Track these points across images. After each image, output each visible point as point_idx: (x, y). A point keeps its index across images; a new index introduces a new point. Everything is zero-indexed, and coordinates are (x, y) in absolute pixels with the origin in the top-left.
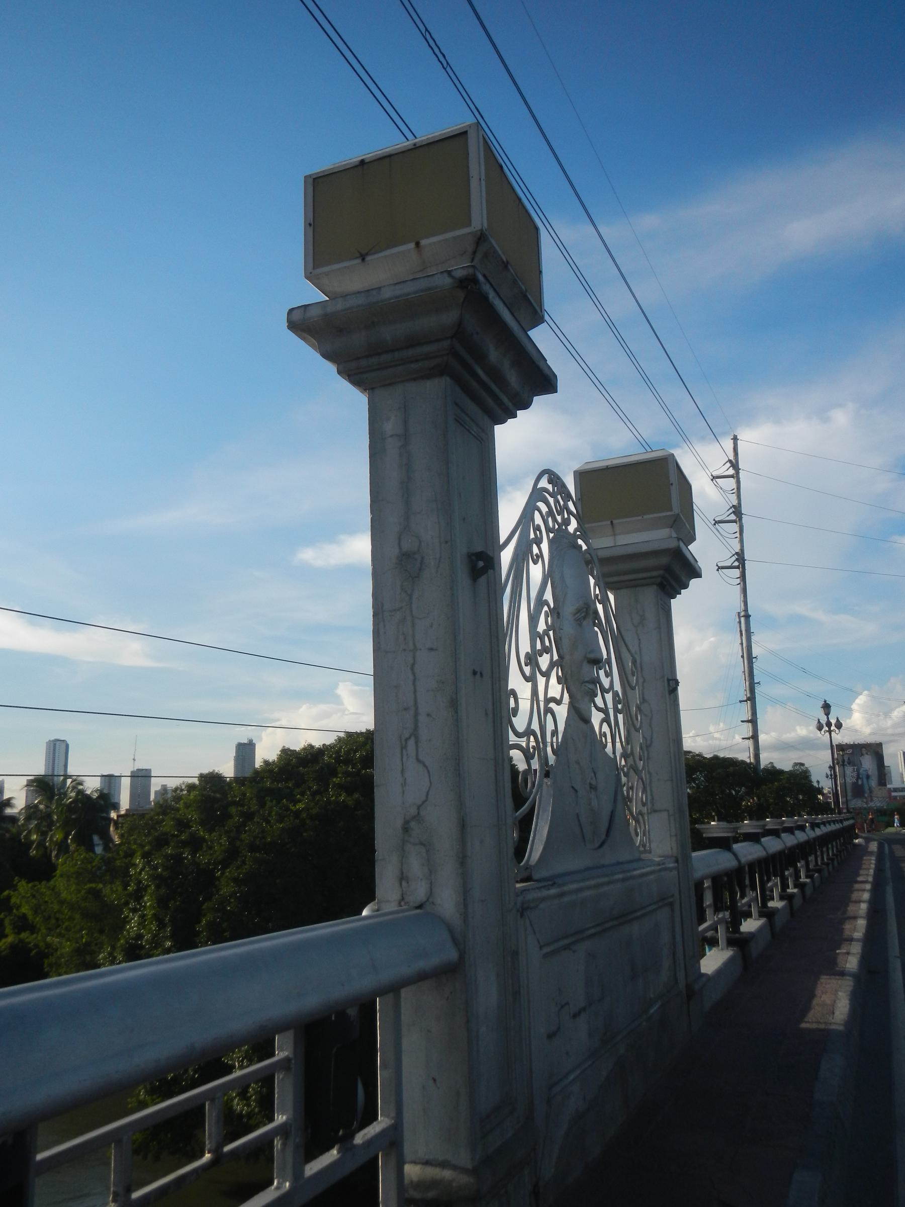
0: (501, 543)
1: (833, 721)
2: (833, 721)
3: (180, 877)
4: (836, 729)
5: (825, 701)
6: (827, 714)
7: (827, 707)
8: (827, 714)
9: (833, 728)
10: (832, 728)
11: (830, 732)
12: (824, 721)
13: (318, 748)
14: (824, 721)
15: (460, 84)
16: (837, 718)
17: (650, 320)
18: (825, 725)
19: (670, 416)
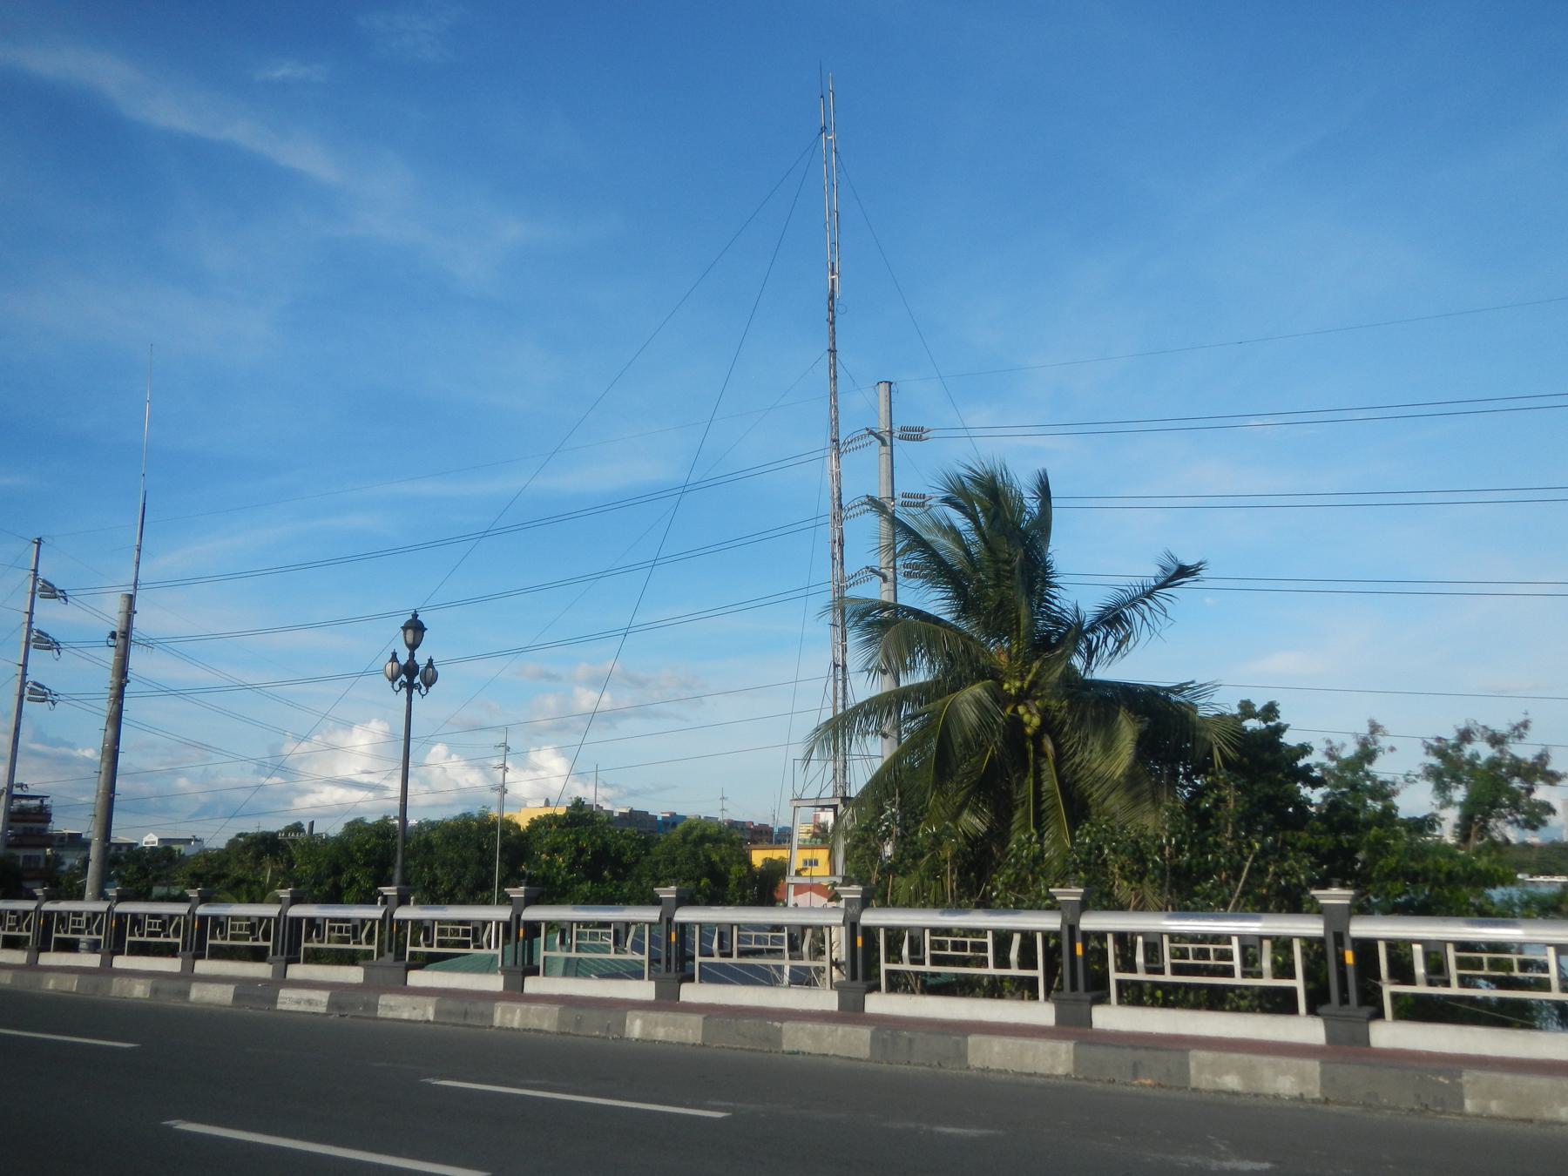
8: (413, 647)
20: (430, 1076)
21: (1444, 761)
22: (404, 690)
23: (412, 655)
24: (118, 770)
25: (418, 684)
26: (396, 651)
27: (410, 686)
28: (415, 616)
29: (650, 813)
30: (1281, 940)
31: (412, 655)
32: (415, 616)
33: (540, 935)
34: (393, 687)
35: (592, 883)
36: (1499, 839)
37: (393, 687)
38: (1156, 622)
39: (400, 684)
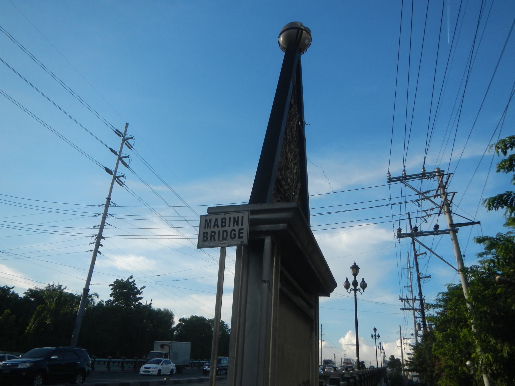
0: (172, 327)
1: (377, 335)
2: (377, 335)
3: (163, 325)
4: (361, 289)
5: (375, 327)
6: (355, 274)
7: (375, 330)
8: (355, 274)
9: (358, 287)
10: (357, 288)
11: (376, 338)
12: (374, 335)
13: (16, 294)
14: (374, 335)
15: (471, 64)
16: (363, 279)
17: (130, 143)
18: (374, 336)
19: (23, 48)
23: (355, 278)
28: (355, 263)
31: (355, 278)
32: (355, 263)
39: (350, 290)
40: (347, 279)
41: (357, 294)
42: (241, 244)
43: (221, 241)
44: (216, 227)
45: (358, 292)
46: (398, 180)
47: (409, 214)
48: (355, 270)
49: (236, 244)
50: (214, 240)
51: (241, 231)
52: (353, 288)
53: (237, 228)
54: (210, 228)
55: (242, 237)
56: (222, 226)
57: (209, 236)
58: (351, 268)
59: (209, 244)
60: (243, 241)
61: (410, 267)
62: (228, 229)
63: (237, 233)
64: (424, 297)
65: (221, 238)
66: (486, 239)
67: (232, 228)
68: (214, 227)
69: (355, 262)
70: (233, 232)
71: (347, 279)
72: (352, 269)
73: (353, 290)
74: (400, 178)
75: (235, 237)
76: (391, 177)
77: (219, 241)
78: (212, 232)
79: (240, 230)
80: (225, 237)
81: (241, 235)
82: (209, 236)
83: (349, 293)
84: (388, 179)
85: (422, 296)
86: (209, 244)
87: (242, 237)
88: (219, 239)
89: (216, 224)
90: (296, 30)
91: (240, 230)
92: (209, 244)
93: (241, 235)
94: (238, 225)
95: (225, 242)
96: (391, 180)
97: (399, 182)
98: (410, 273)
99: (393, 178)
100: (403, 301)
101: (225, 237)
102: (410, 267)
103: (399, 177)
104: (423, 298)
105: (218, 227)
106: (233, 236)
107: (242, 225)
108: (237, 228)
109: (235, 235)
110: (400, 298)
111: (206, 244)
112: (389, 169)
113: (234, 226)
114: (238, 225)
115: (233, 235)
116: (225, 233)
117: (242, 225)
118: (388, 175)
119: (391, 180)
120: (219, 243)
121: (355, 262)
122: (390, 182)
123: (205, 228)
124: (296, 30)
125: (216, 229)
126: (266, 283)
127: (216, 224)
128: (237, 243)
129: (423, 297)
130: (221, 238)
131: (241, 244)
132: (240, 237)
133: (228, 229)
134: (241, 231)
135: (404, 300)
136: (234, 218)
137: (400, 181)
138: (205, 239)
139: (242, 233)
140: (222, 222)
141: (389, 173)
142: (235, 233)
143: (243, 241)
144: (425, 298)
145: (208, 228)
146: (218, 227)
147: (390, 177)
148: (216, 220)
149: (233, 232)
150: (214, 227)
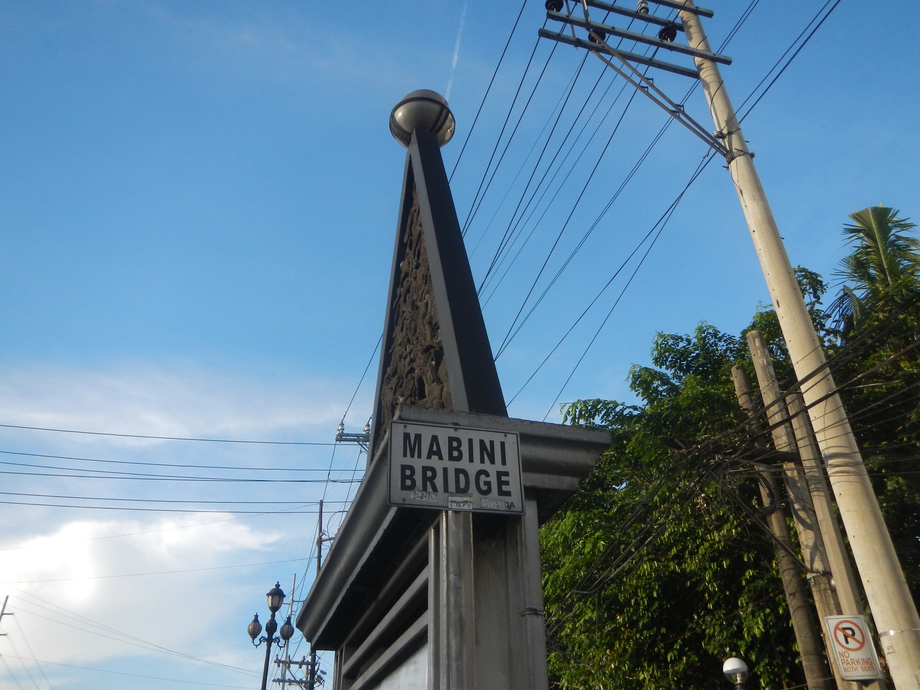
6: (274, 609)
8: (274, 609)
20: (789, 487)
21: (651, 402)
22: (264, 645)
23: (273, 616)
24: (809, 373)
25: (278, 638)
26: (258, 614)
27: (270, 641)
28: (278, 586)
29: (726, 119)
30: (851, 552)
31: (273, 616)
32: (278, 586)
33: (838, 615)
34: (253, 642)
35: (754, 636)
36: (770, 542)
37: (253, 642)
38: (857, 238)
39: (260, 640)
40: (256, 616)
41: (272, 648)
42: (507, 509)
43: (452, 494)
44: (435, 458)
45: (274, 645)
46: (355, 440)
47: (321, 503)
48: (277, 598)
49: (496, 508)
50: (435, 489)
51: (504, 478)
52: (266, 636)
53: (492, 469)
54: (420, 456)
55: (508, 494)
56: (451, 458)
57: (418, 477)
58: (268, 595)
59: (422, 498)
60: (512, 503)
61: (293, 601)
62: (472, 469)
63: (493, 479)
64: (319, 658)
65: (452, 487)
66: (625, 559)
67: (477, 466)
68: (429, 457)
69: (278, 582)
70: (483, 478)
71: (256, 616)
72: (270, 597)
73: (266, 640)
74: (358, 437)
75: (489, 491)
76: (344, 432)
77: (446, 494)
78: (425, 469)
79: (500, 474)
80: (462, 485)
81: (505, 488)
82: (418, 477)
83: (257, 646)
84: (338, 435)
85: (316, 657)
86: (422, 498)
87: (508, 494)
88: (446, 490)
89: (435, 449)
90: (437, 108)
91: (500, 474)
92: (420, 499)
93: (505, 488)
94: (492, 461)
95: (465, 499)
96: (342, 437)
97: (356, 443)
98: (292, 611)
99: (348, 435)
100: (281, 664)
101: (462, 485)
102: (293, 600)
103: (358, 436)
104: (316, 660)
105: (441, 458)
106: (484, 488)
107: (504, 462)
108: (492, 469)
109: (488, 484)
110: (277, 658)
111: (412, 497)
112: (344, 416)
113: (482, 461)
114: (492, 461)
115: (485, 485)
116: (462, 477)
117: (504, 462)
118: (340, 428)
119: (342, 437)
120: (450, 498)
121: (278, 582)
122: (340, 441)
123: (405, 455)
124: (437, 108)
125: (434, 462)
126: (539, 616)
127: (435, 449)
128: (497, 506)
129: (317, 658)
130: (452, 487)
131: (507, 509)
132: (501, 493)
133: (472, 469)
134: (504, 478)
135: (283, 662)
136: (482, 442)
137: (358, 442)
138: (408, 483)
139: (507, 483)
140: (451, 449)
141: (342, 424)
142: (488, 479)
143: (512, 503)
144: (320, 661)
145: (412, 456)
146: (441, 458)
147: (342, 432)
148: (435, 439)
149: (483, 478)
150: (429, 457)
